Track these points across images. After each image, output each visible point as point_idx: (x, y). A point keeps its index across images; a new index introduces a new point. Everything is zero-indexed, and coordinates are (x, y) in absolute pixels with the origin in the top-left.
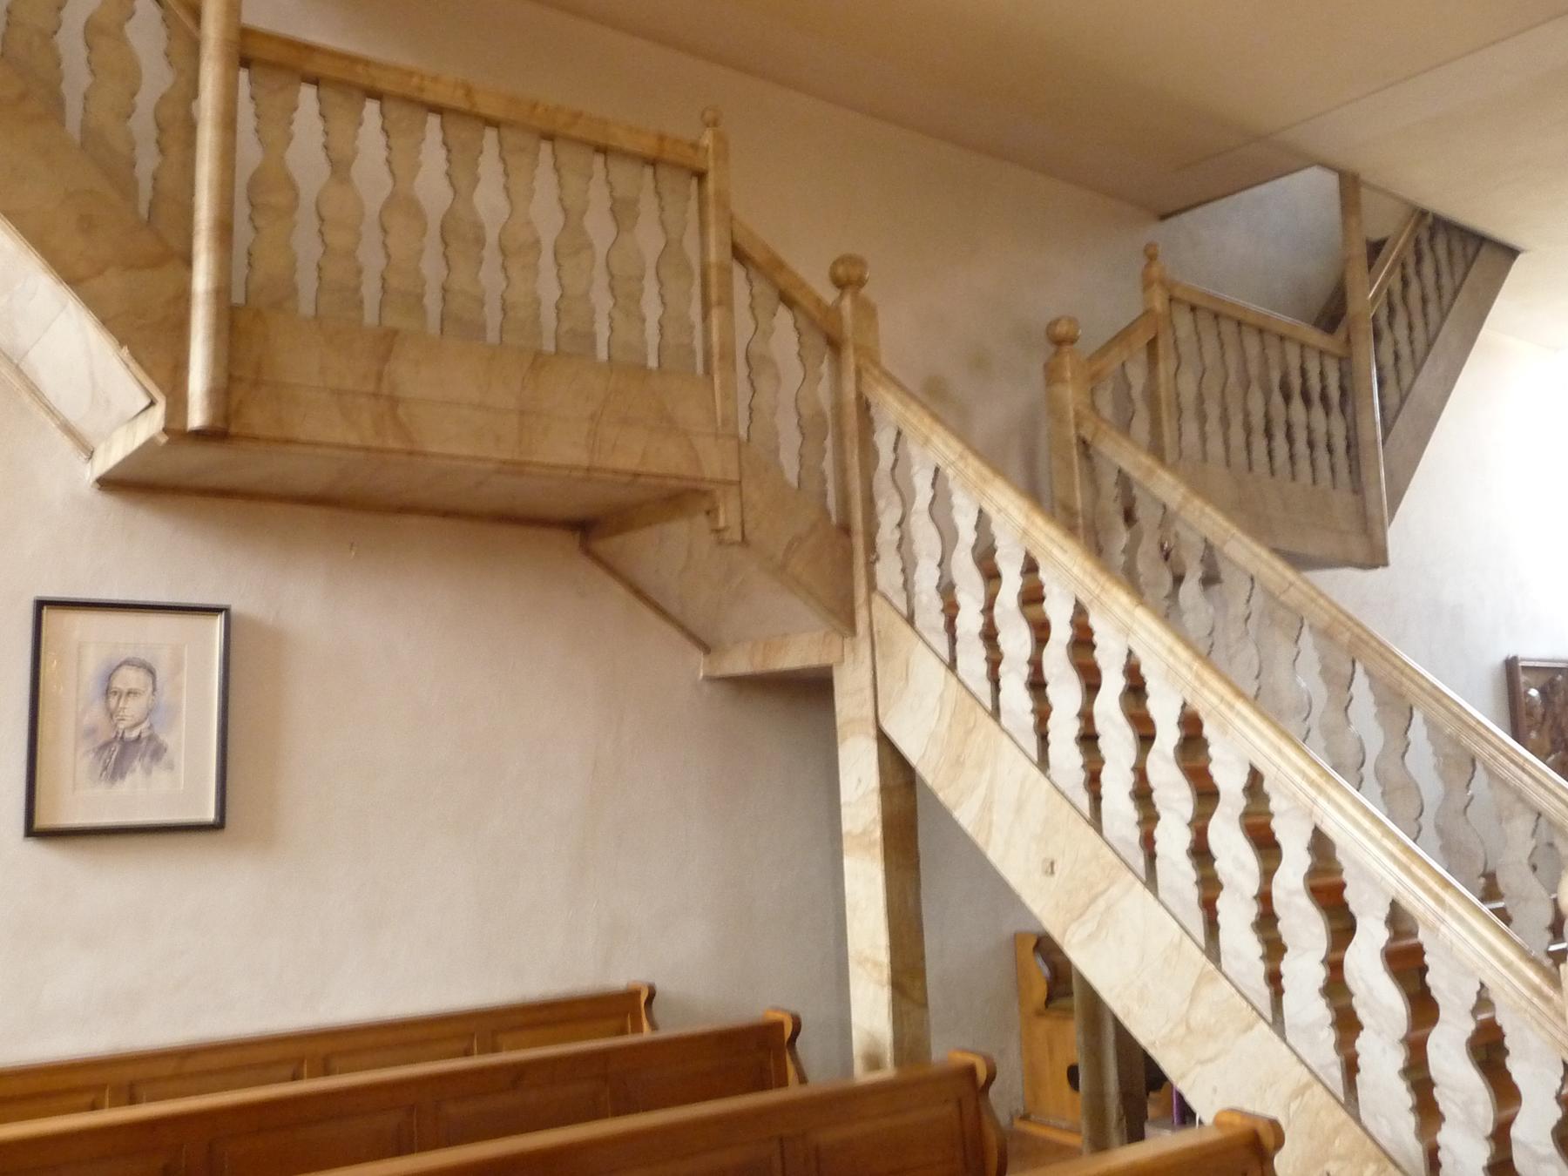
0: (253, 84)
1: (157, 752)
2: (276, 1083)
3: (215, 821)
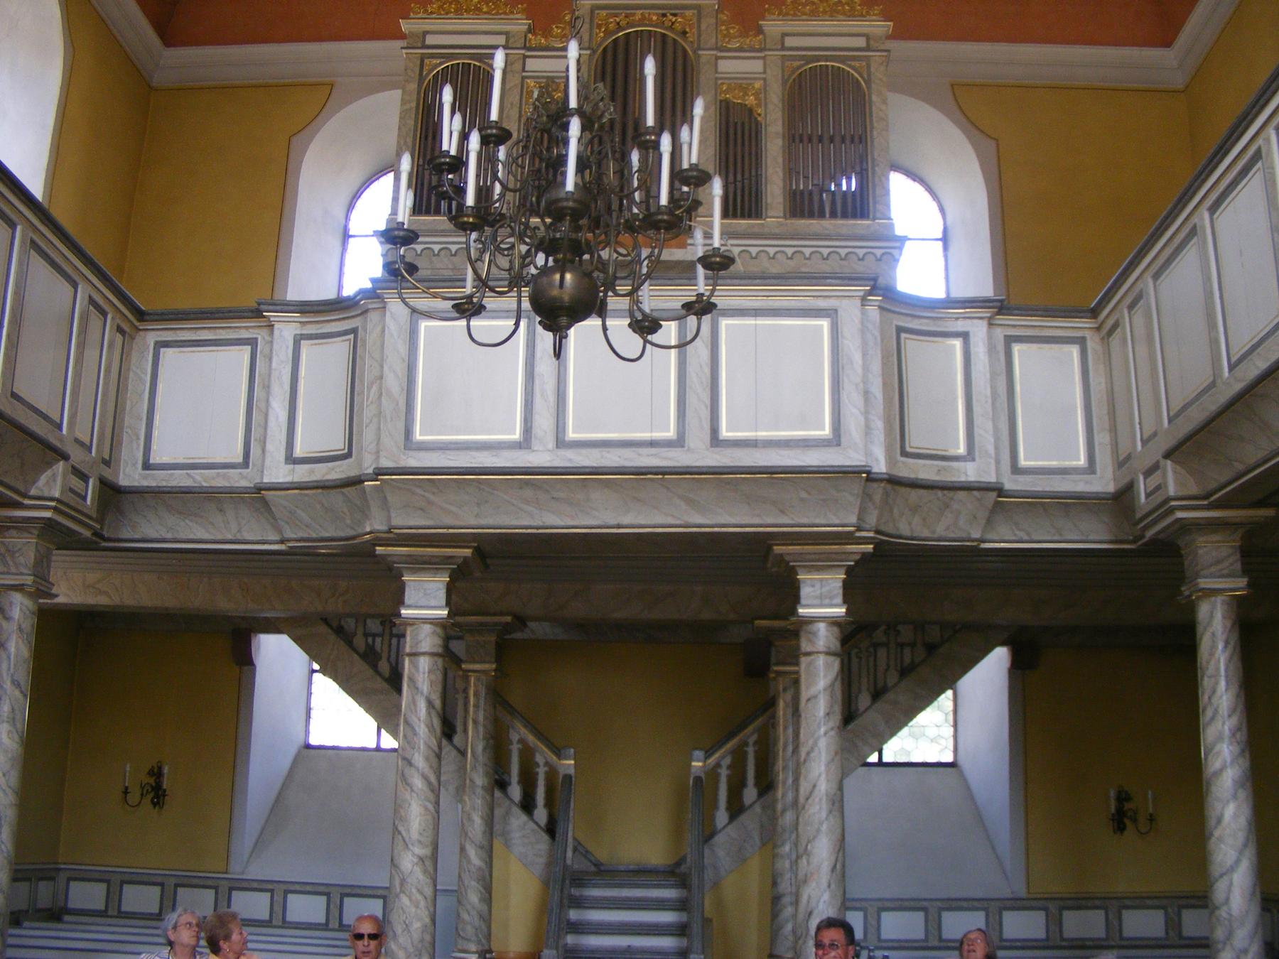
1: (374, 232)
2: (276, 42)
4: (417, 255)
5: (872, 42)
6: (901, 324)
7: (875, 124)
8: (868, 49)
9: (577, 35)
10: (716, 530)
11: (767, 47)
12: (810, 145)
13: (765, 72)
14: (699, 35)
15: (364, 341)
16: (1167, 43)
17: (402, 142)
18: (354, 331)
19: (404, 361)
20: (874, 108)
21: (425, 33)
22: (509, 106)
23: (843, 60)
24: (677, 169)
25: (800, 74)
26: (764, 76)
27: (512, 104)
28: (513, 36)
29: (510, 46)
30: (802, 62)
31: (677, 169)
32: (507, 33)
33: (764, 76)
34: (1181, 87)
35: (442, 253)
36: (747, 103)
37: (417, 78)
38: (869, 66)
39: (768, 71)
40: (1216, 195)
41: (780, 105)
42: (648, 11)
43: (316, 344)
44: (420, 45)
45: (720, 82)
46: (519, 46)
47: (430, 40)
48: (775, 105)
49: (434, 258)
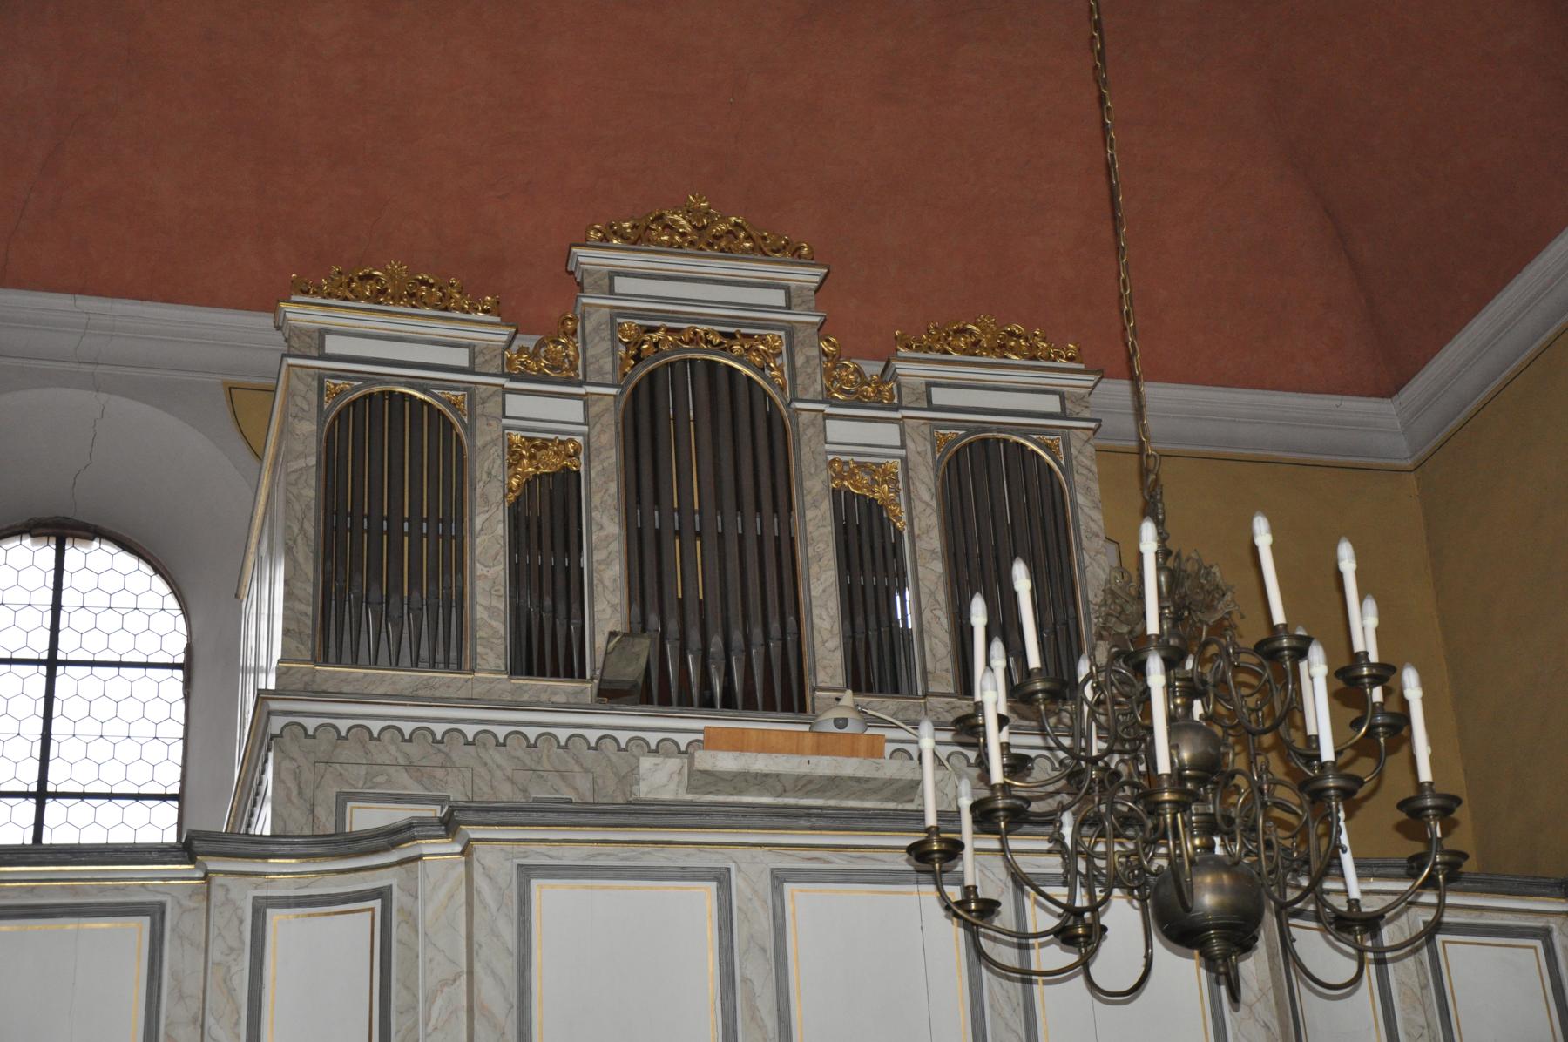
0: (982, 959)
3: (1259, 515)
4: (340, 737)
5: (1069, 405)
6: (1444, 939)
7: (1085, 542)
8: (1063, 415)
9: (1374, 704)
10: (403, 334)
11: (904, 403)
12: (739, 513)
13: (903, 446)
14: (793, 377)
15: (411, 919)
16: (1388, 390)
17: (296, 529)
18: (383, 894)
19: (511, 954)
20: (1081, 518)
21: (323, 333)
22: (485, 477)
23: (1026, 431)
24: (1204, 699)
25: (957, 452)
26: (902, 452)
27: (489, 474)
28: (481, 352)
29: (477, 370)
30: (1063, 462)
31: (1204, 699)
32: (470, 347)
33: (902, 452)
34: (1408, 463)
35: (387, 736)
36: (876, 496)
37: (315, 410)
38: (1067, 446)
39: (909, 443)
40: (559, 646)
41: (934, 503)
42: (704, 327)
43: (309, 915)
44: (315, 353)
45: (831, 457)
46: (493, 371)
47: (333, 345)
48: (925, 502)
49: (372, 745)
